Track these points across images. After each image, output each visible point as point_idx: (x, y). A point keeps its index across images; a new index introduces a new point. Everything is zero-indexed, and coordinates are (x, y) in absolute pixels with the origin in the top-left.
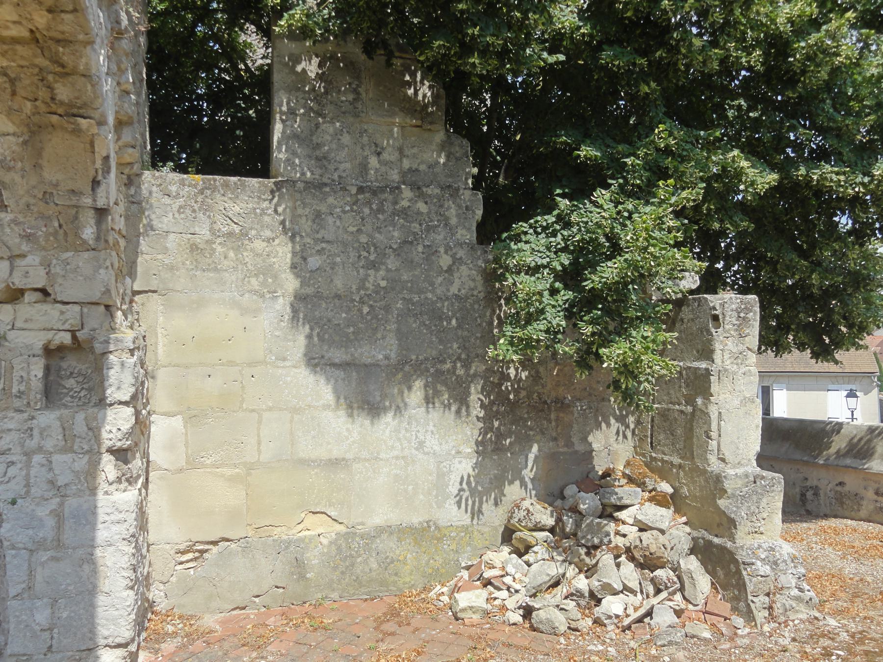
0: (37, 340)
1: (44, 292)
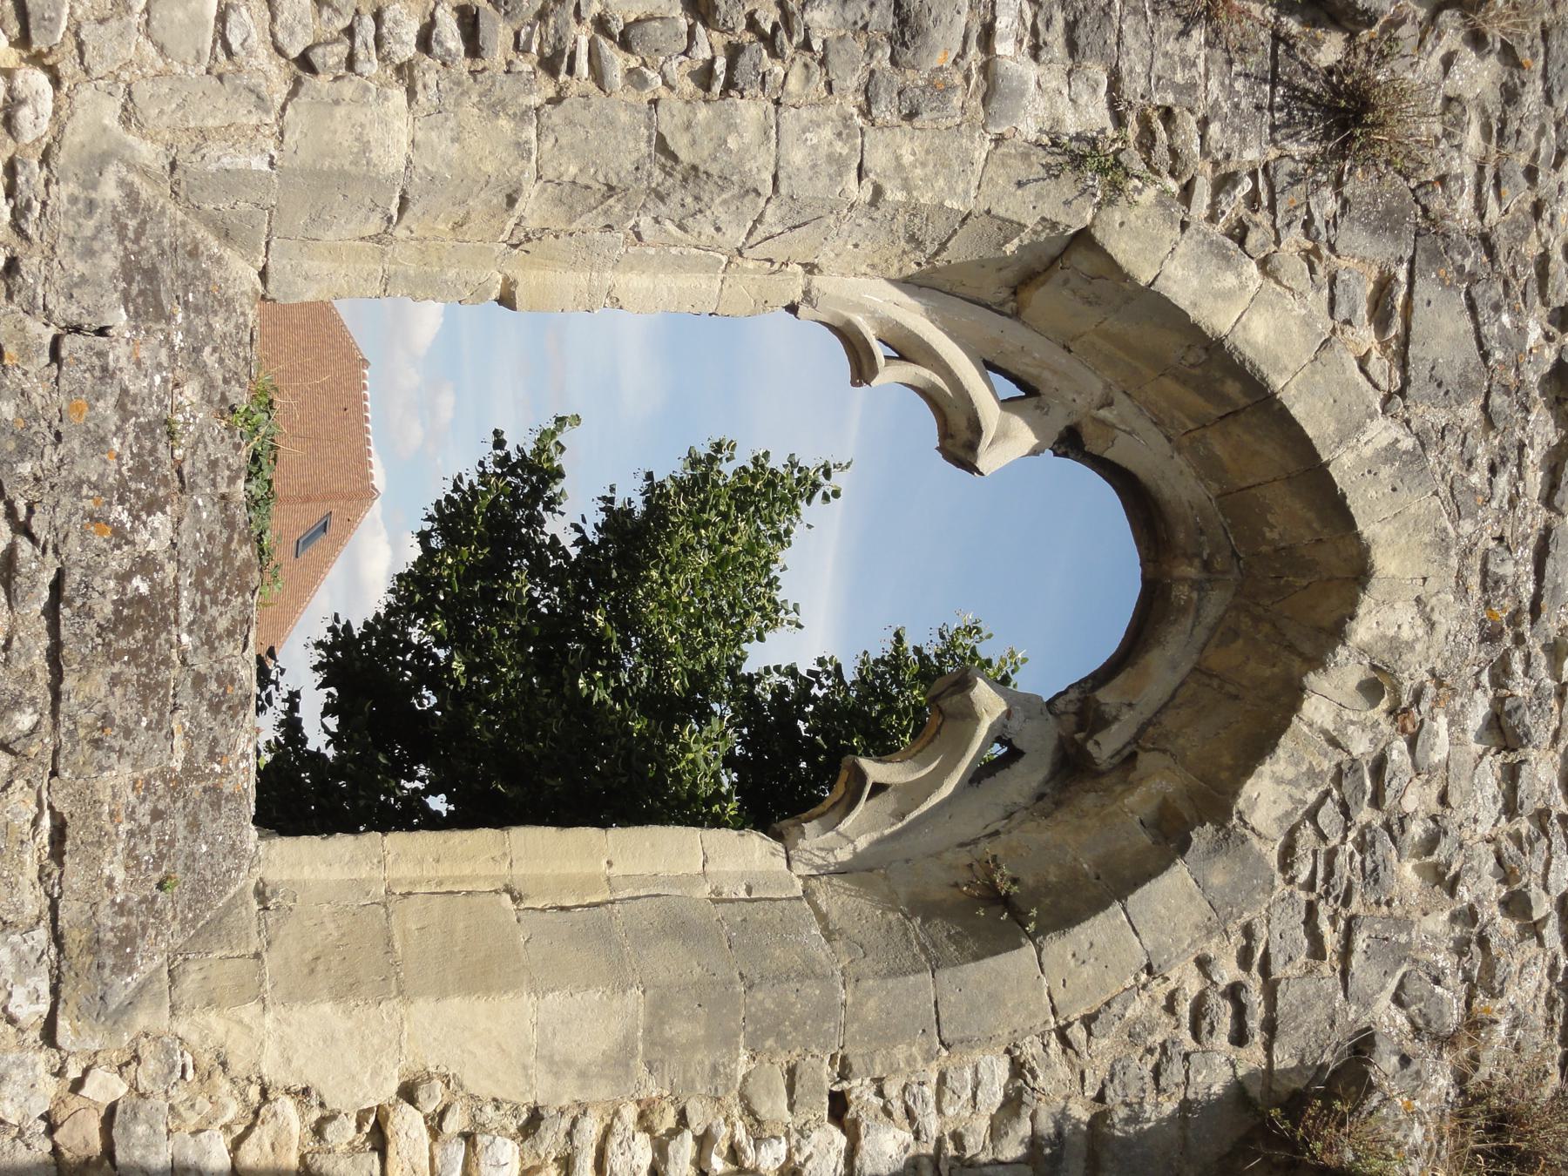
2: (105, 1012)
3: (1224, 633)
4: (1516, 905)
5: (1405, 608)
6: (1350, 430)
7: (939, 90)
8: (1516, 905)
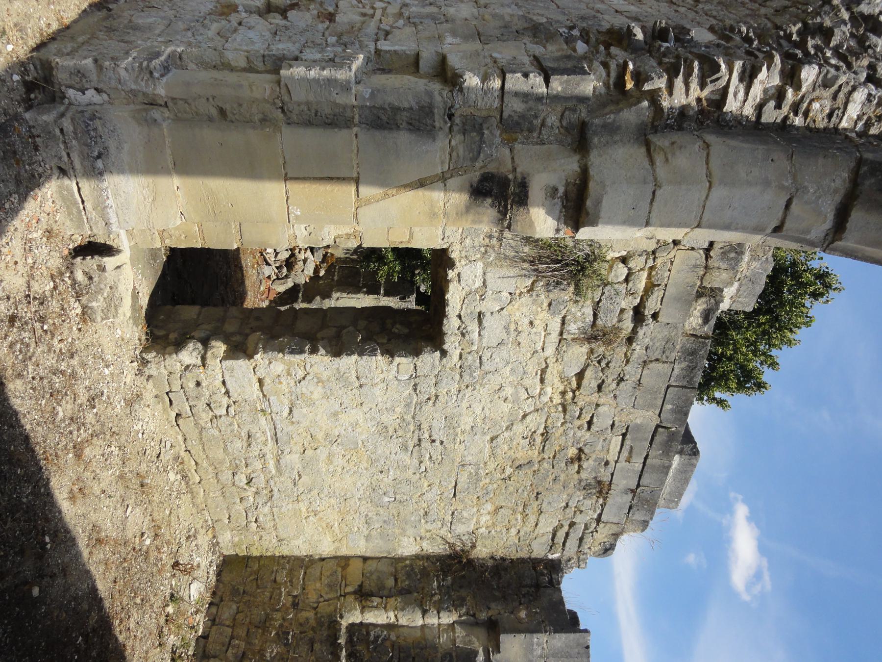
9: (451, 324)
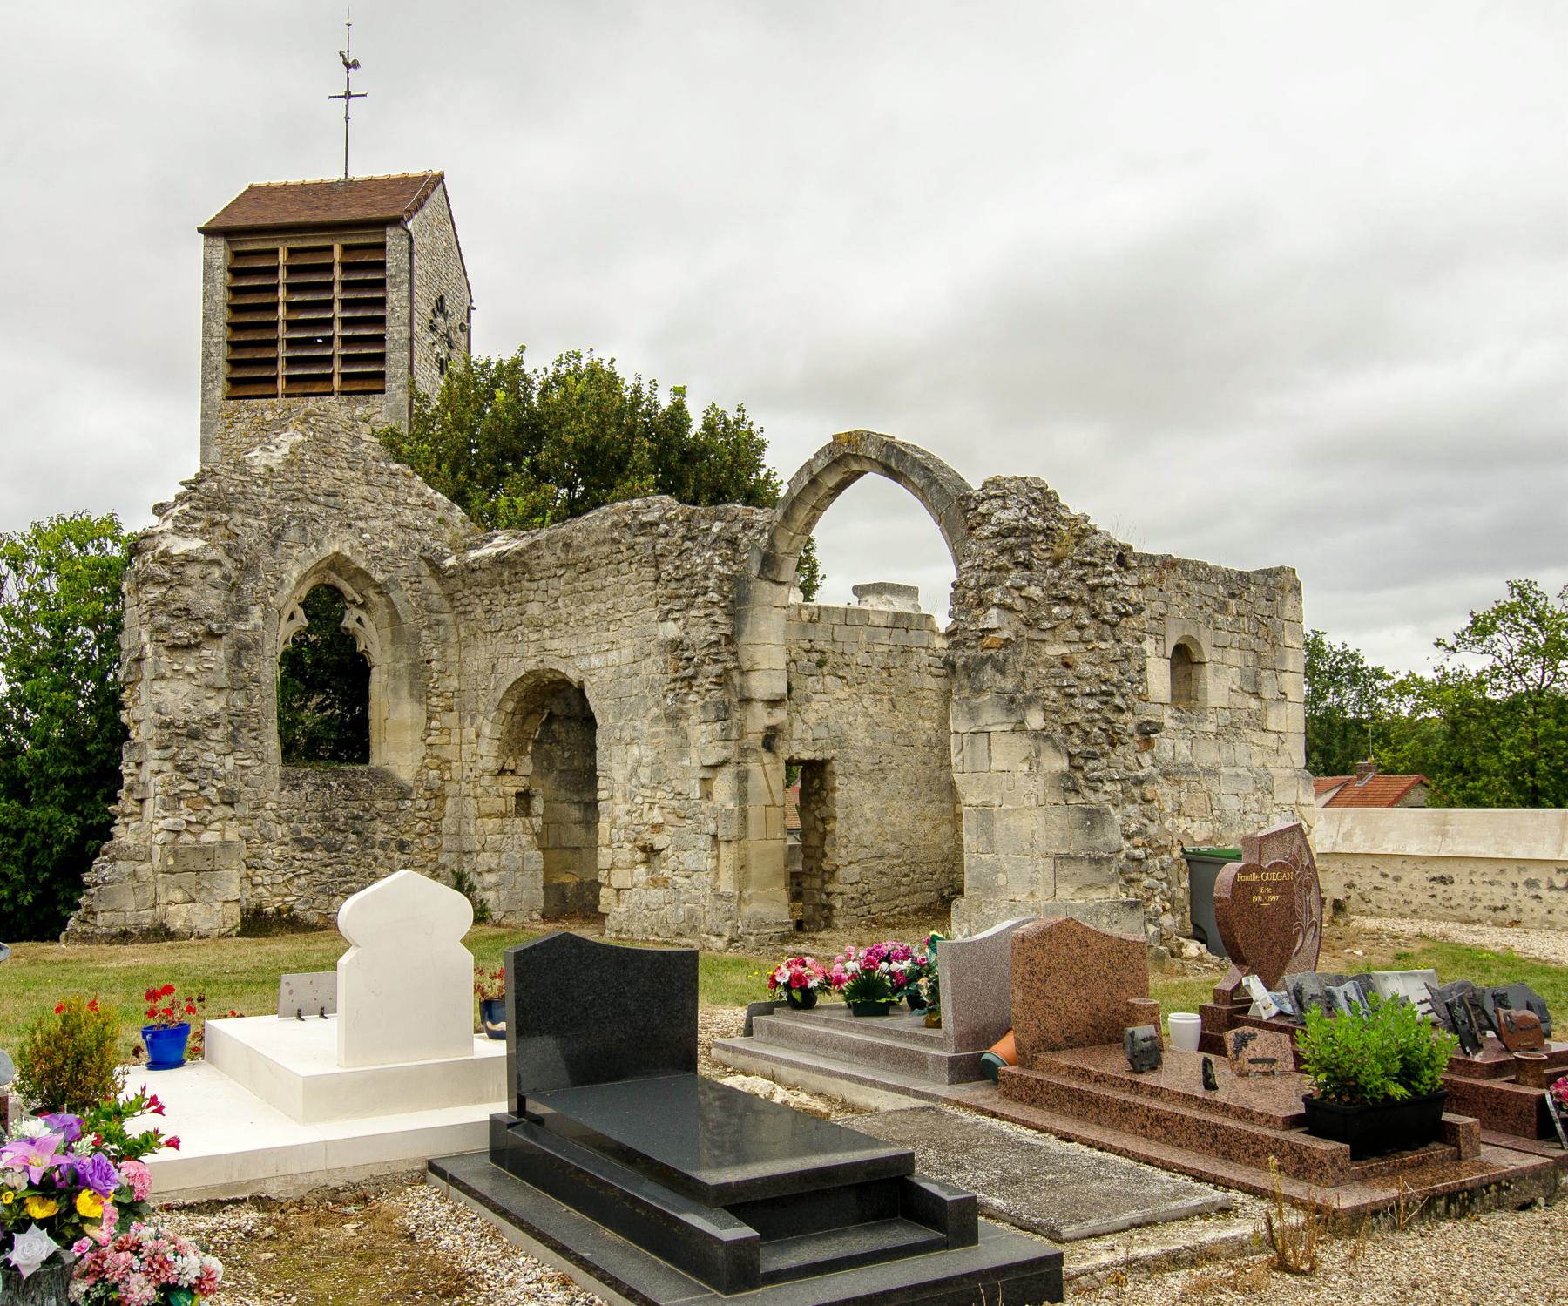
0: (514, 790)
1: (513, 772)
2: (411, 791)
3: (340, 575)
4: (394, 516)
5: (339, 544)
6: (313, 556)
7: (256, 641)
8: (394, 516)
9: (819, 756)
